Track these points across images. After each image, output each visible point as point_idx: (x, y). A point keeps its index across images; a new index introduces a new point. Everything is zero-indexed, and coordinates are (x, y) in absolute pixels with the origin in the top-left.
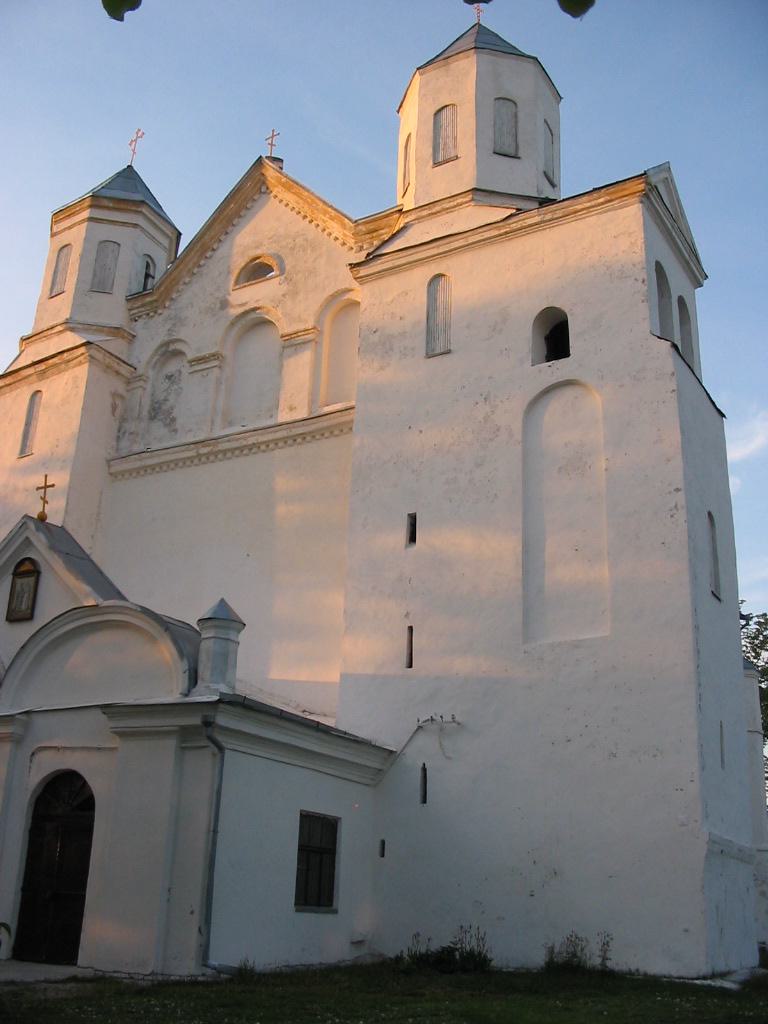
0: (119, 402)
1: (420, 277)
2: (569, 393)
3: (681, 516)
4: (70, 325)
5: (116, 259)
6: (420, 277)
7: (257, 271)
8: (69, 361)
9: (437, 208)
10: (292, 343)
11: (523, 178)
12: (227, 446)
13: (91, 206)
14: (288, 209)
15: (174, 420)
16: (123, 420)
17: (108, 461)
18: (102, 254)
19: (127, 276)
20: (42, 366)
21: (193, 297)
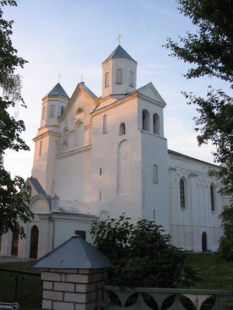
0: (57, 142)
1: (102, 115)
2: (125, 142)
3: (141, 169)
4: (46, 126)
5: (54, 109)
6: (102, 115)
7: (80, 111)
8: (45, 135)
9: (104, 99)
10: (86, 128)
11: (123, 89)
12: (76, 152)
13: (48, 97)
14: (84, 95)
15: (68, 145)
16: (59, 146)
17: (56, 156)
18: (52, 107)
19: (57, 112)
20: (41, 136)
21: (69, 117)
